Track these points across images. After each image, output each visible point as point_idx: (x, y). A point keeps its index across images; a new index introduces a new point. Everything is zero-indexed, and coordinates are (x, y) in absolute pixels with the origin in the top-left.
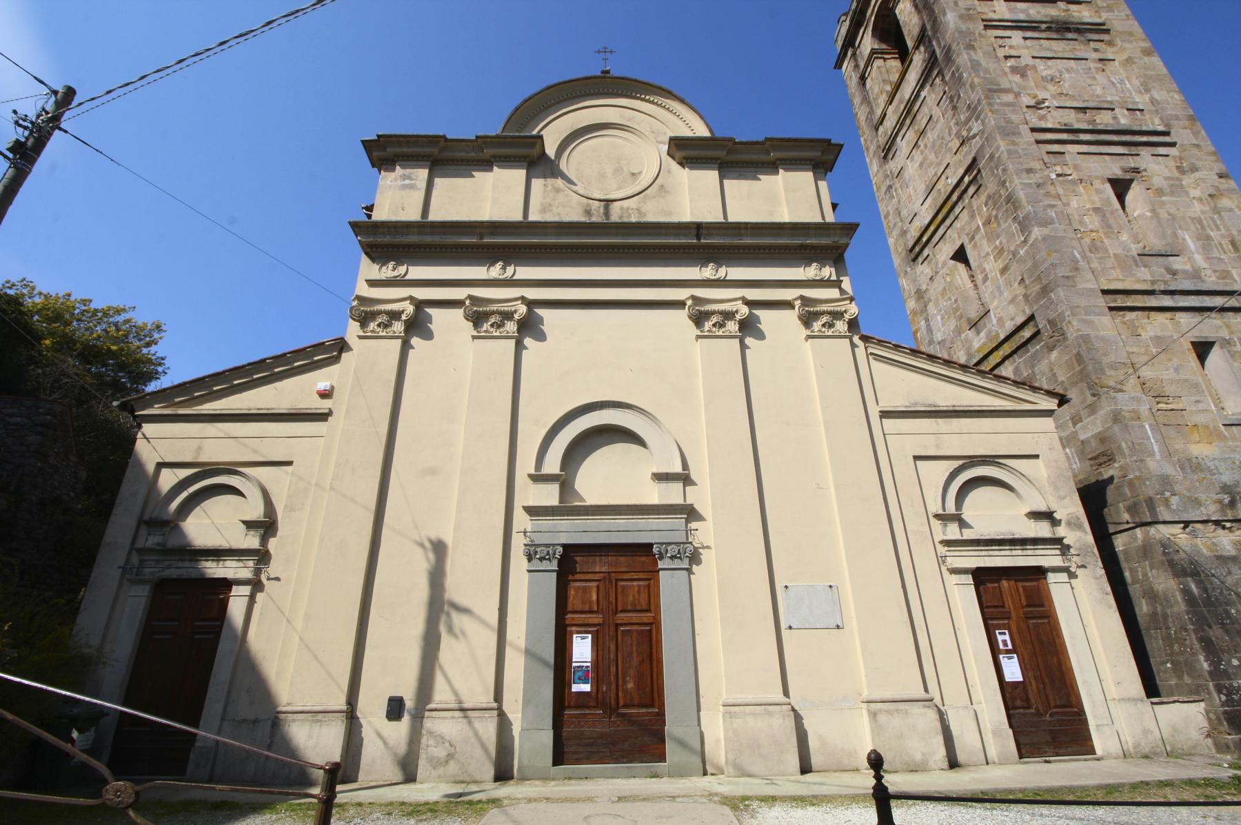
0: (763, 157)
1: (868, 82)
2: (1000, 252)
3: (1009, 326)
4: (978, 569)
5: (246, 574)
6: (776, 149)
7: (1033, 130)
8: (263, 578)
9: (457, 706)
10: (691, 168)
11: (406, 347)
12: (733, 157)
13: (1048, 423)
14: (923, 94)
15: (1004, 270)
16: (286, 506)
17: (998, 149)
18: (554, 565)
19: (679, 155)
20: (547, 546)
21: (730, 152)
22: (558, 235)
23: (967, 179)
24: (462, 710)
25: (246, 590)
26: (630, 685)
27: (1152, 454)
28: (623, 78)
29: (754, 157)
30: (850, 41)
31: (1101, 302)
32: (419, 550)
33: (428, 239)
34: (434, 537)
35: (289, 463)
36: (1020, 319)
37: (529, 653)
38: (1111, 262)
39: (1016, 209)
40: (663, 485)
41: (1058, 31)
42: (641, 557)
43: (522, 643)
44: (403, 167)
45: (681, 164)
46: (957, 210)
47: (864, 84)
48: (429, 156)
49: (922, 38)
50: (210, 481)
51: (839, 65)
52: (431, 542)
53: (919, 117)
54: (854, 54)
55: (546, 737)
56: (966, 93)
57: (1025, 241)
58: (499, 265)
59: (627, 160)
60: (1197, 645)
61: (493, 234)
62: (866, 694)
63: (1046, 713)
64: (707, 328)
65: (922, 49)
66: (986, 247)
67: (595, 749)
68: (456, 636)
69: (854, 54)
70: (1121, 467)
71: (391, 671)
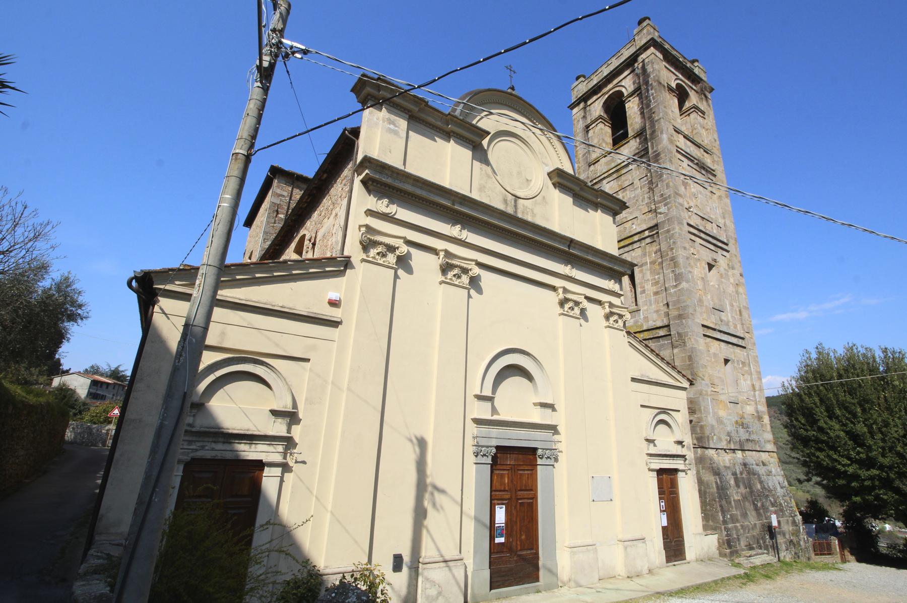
0: (594, 199)
1: (591, 133)
2: (657, 283)
3: (651, 324)
4: (661, 469)
5: (278, 458)
6: (602, 197)
7: (728, 251)
9: (441, 559)
10: (560, 191)
13: (683, 394)
14: (631, 167)
15: (656, 293)
16: (306, 399)
17: (674, 229)
18: (489, 460)
19: (556, 179)
20: (488, 447)
22: (499, 219)
23: (647, 233)
24: (445, 561)
25: (278, 471)
26: (523, 537)
28: (530, 105)
30: (585, 98)
31: (702, 331)
32: (409, 444)
33: (419, 192)
34: (418, 435)
36: (659, 324)
37: (477, 520)
38: (704, 309)
39: (675, 267)
40: (543, 410)
42: (529, 455)
43: (473, 513)
44: (389, 111)
45: (554, 184)
46: (635, 246)
47: (587, 132)
48: (409, 111)
49: (641, 134)
50: (243, 368)
51: (572, 107)
52: (417, 438)
53: (623, 178)
54: (585, 108)
55: (487, 574)
56: (662, 186)
57: (676, 286)
58: (458, 227)
59: (521, 168)
60: (719, 509)
61: (461, 204)
62: (620, 537)
63: (674, 546)
64: (566, 309)
65: (638, 140)
66: (648, 276)
67: (507, 578)
68: (438, 510)
69: (585, 108)
70: (698, 418)
71: (395, 538)
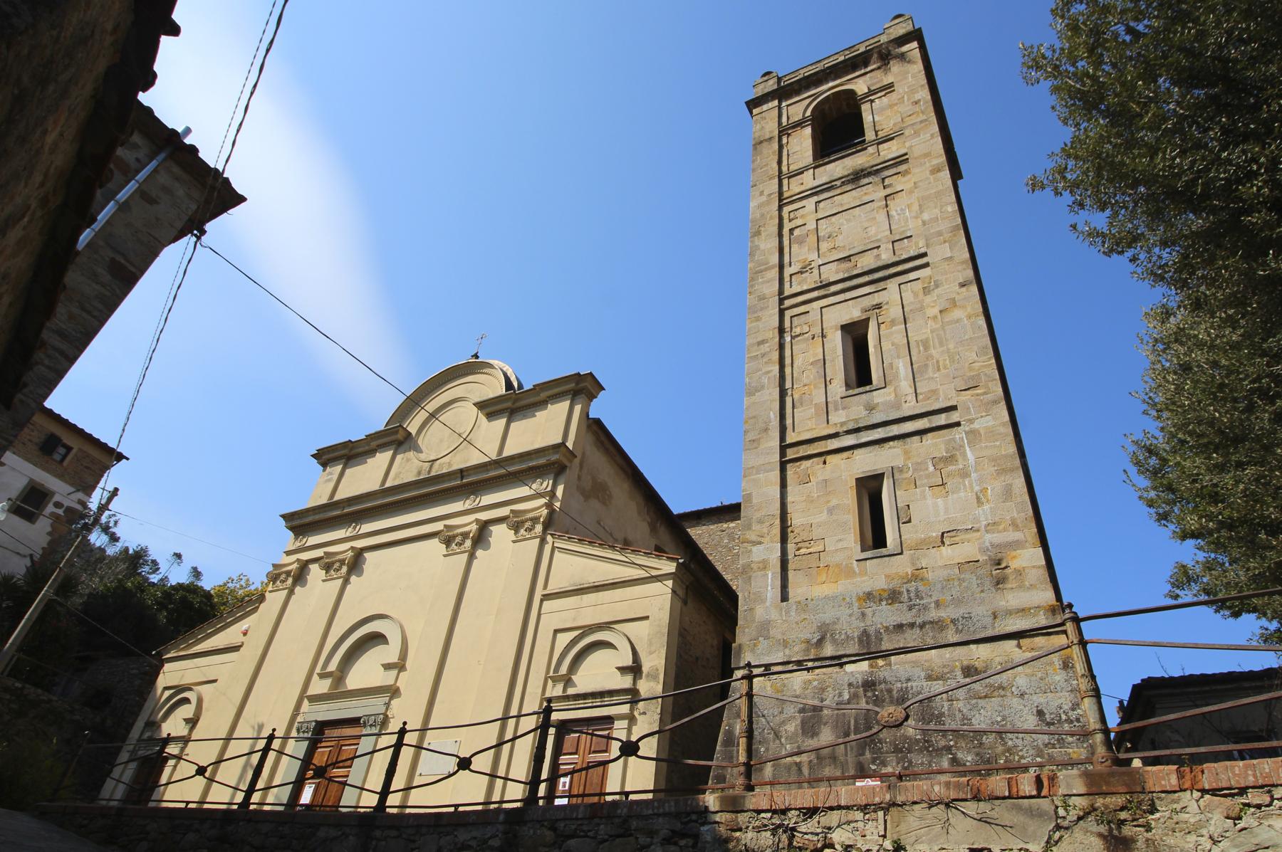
8: (636, 713)
11: (472, 556)
12: (518, 404)
21: (515, 401)
22: (384, 497)
25: (625, 723)
27: (763, 601)
29: (532, 400)
35: (215, 681)
41: (849, 182)
61: (349, 506)
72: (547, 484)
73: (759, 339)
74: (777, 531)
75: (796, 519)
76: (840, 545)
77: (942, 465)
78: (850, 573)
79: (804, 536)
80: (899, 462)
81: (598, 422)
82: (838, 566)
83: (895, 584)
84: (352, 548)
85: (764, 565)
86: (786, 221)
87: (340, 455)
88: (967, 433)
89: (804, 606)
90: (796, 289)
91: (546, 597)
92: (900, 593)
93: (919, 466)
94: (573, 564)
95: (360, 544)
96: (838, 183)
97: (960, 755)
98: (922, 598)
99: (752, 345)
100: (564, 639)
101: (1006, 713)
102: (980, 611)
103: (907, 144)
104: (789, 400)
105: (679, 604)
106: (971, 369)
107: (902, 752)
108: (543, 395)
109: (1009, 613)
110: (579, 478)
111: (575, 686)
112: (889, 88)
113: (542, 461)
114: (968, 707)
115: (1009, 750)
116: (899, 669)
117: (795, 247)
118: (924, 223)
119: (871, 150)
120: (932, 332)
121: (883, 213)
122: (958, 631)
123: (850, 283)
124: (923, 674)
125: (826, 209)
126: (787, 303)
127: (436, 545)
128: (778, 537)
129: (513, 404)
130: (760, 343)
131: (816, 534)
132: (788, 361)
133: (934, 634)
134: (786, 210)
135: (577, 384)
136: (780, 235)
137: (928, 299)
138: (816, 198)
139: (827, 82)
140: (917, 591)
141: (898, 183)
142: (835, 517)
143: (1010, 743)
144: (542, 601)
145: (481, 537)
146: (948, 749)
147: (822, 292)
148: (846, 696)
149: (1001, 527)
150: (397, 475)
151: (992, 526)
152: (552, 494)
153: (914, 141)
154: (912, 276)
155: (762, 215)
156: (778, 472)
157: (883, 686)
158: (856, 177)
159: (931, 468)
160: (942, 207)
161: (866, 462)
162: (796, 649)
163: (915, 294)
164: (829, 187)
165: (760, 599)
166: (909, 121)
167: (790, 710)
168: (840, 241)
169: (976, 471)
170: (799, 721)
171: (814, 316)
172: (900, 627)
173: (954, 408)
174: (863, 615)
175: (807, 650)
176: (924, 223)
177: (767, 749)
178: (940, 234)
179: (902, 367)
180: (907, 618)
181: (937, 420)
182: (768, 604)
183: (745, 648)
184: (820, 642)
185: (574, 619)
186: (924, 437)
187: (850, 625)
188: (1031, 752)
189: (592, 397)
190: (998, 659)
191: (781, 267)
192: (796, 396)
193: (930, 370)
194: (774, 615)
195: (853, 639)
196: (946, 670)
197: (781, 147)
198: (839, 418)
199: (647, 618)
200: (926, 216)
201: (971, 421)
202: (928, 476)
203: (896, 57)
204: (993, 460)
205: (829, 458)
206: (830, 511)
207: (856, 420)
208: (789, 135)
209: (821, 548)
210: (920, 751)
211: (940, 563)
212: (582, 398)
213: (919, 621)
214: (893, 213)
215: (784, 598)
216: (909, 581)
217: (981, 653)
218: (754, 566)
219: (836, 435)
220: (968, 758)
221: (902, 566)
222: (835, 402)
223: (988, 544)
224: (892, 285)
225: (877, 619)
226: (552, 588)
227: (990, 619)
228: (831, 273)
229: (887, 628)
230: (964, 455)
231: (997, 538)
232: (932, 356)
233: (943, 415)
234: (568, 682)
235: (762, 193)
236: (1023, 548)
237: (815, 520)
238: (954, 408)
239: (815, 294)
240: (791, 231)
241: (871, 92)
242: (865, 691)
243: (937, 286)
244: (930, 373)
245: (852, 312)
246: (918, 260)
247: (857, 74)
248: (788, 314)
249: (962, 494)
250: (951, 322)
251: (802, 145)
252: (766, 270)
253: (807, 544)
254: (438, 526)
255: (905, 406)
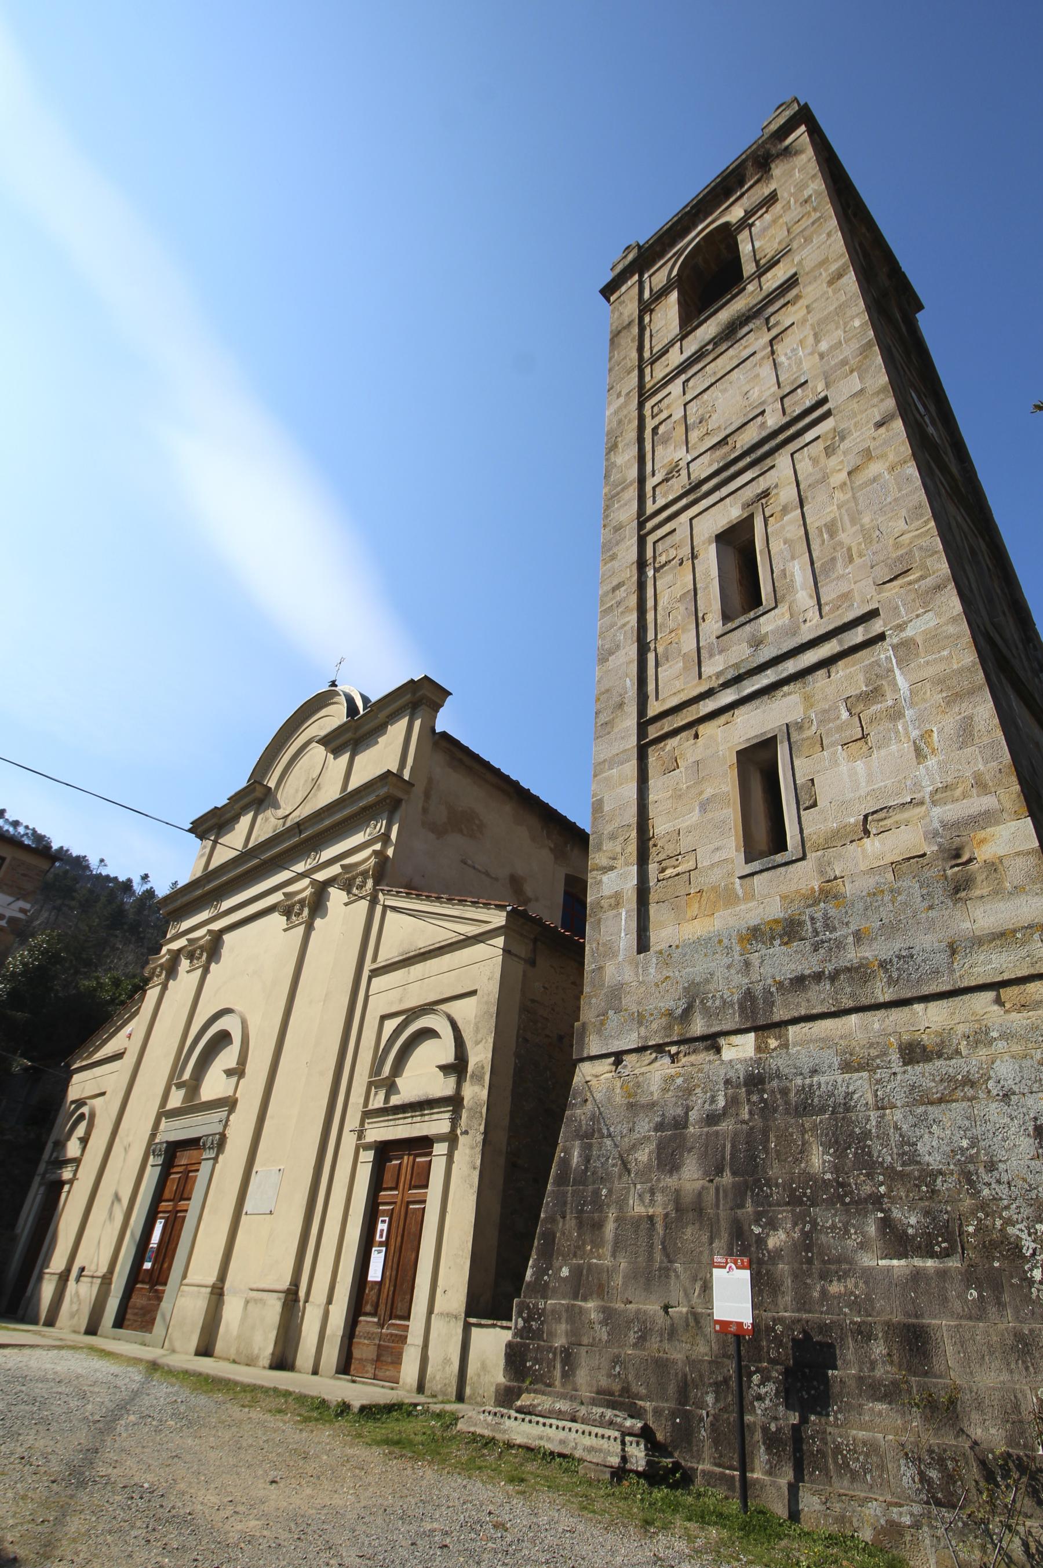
21: (357, 729)
22: (236, 867)
27: (615, 955)
72: (381, 826)
73: (615, 583)
74: (632, 848)
75: (660, 826)
76: (717, 857)
77: (860, 707)
78: (729, 898)
79: (670, 849)
80: (795, 715)
81: (444, 735)
82: (714, 889)
83: (792, 910)
84: (209, 931)
85: (617, 900)
86: (648, 419)
87: (210, 826)
88: (894, 647)
89: (666, 957)
90: (661, 502)
91: (375, 973)
92: (801, 924)
93: (826, 716)
94: (405, 928)
95: (216, 926)
96: (710, 347)
97: (896, 1214)
98: (834, 929)
99: (606, 594)
100: (390, 1025)
101: (978, 1131)
102: (927, 942)
103: (797, 260)
104: (651, 657)
105: (519, 967)
106: (897, 546)
107: (801, 1203)
108: (382, 716)
109: (978, 942)
110: (425, 811)
111: (399, 1093)
112: (772, 199)
113: (371, 799)
114: (911, 1120)
115: (983, 1206)
116: (811, 1049)
117: (659, 449)
118: (822, 356)
119: (750, 288)
120: (839, 507)
121: (768, 366)
122: (891, 982)
123: (725, 474)
124: (836, 1061)
125: (697, 385)
126: (649, 525)
127: (277, 920)
128: (634, 858)
129: (357, 732)
130: (614, 589)
131: (685, 845)
132: (650, 603)
133: (851, 988)
134: (648, 405)
135: (414, 693)
136: (641, 440)
137: (833, 462)
138: (683, 377)
139: (695, 226)
140: (826, 917)
141: (786, 317)
142: (710, 815)
143: (986, 1192)
144: (370, 979)
145: (317, 904)
146: (876, 1200)
147: (691, 497)
148: (721, 1103)
149: (958, 793)
150: (256, 839)
151: (943, 793)
152: (385, 838)
153: (805, 253)
154: (809, 436)
155: (620, 422)
156: (634, 762)
157: (775, 1083)
158: (730, 333)
159: (845, 715)
160: (846, 324)
161: (750, 724)
162: (654, 1026)
163: (815, 461)
164: (699, 355)
165: (611, 952)
166: (797, 229)
167: (644, 1126)
168: (712, 424)
169: (912, 705)
170: (653, 1146)
171: (683, 532)
172: (799, 982)
173: (874, 614)
174: (747, 964)
175: (669, 1027)
176: (822, 356)
177: (610, 1191)
178: (844, 362)
179: (799, 572)
180: (809, 964)
181: (853, 637)
182: (620, 958)
183: (590, 1028)
184: (686, 1014)
185: (401, 1000)
186: (833, 669)
187: (727, 984)
188: (1026, 1211)
189: (436, 707)
190: (961, 1029)
191: (642, 480)
192: (660, 650)
193: (839, 564)
194: (628, 975)
195: (732, 1005)
196: (874, 1052)
197: (642, 329)
198: (715, 666)
199: (474, 993)
200: (823, 346)
201: (901, 627)
202: (840, 729)
203: (778, 156)
204: (940, 681)
205: (702, 729)
206: (704, 807)
207: (736, 666)
208: (652, 311)
209: (691, 865)
210: (831, 1203)
211: (863, 867)
212: (424, 709)
213: (830, 968)
214: (782, 359)
215: (643, 945)
216: (816, 903)
217: (931, 1019)
218: (604, 903)
219: (709, 693)
220: (912, 1220)
221: (803, 877)
222: (711, 644)
223: (936, 825)
224: (783, 459)
225: (767, 970)
226: (381, 961)
227: (943, 958)
228: (702, 468)
229: (780, 985)
230: (894, 684)
231: (951, 811)
232: (841, 544)
233: (860, 629)
234: (391, 1088)
235: (619, 395)
236: (997, 823)
237: (683, 824)
238: (874, 614)
239: (684, 502)
240: (655, 430)
241: (749, 214)
242: (749, 1093)
243: (843, 439)
244: (840, 569)
245: (730, 513)
246: (819, 410)
247: (731, 200)
248: (650, 540)
249: (894, 747)
250: (862, 487)
251: (667, 316)
252: (623, 490)
253: (673, 862)
254: (277, 897)
255: (804, 628)
